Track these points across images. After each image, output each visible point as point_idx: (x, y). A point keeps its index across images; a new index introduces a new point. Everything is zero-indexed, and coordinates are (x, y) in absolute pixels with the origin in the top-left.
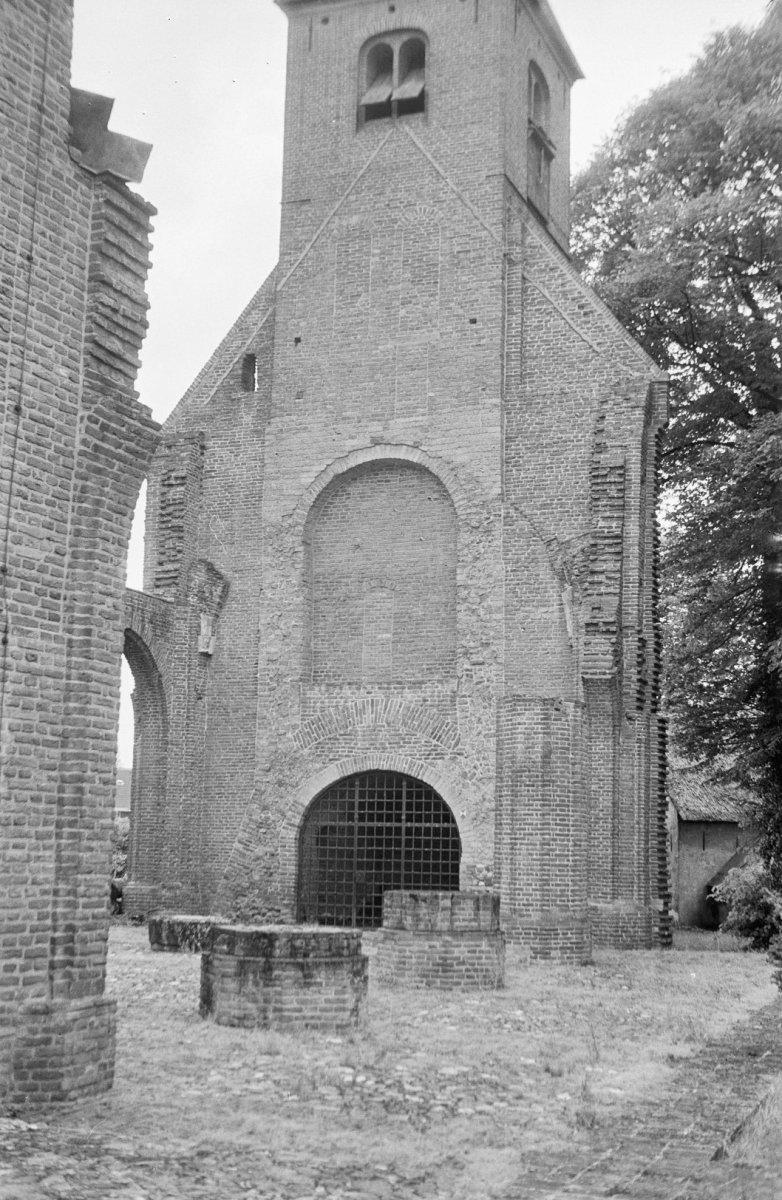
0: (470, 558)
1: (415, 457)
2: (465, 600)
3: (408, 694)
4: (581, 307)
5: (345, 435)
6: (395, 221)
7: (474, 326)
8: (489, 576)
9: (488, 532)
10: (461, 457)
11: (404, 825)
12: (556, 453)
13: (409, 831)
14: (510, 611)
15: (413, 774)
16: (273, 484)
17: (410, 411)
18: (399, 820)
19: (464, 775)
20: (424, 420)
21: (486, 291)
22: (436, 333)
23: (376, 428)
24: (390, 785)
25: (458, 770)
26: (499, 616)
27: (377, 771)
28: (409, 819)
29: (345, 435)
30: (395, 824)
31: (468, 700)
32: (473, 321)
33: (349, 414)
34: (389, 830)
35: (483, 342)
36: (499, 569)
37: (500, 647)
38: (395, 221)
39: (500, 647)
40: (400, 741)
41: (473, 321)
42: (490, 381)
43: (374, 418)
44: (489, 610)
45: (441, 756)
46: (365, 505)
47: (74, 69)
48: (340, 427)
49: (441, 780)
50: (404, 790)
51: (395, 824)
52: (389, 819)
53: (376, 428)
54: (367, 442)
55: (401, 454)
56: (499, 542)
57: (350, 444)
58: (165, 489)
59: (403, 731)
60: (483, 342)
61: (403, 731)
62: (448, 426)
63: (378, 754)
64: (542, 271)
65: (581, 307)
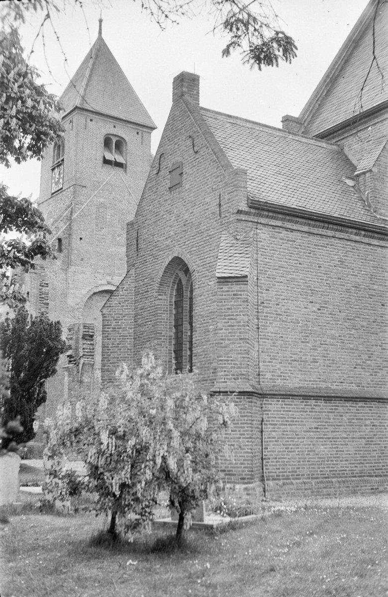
16: (72, 291)
23: (109, 278)
43: (109, 275)
48: (97, 275)
53: (109, 278)
54: (106, 283)
57: (100, 282)
58: (41, 288)
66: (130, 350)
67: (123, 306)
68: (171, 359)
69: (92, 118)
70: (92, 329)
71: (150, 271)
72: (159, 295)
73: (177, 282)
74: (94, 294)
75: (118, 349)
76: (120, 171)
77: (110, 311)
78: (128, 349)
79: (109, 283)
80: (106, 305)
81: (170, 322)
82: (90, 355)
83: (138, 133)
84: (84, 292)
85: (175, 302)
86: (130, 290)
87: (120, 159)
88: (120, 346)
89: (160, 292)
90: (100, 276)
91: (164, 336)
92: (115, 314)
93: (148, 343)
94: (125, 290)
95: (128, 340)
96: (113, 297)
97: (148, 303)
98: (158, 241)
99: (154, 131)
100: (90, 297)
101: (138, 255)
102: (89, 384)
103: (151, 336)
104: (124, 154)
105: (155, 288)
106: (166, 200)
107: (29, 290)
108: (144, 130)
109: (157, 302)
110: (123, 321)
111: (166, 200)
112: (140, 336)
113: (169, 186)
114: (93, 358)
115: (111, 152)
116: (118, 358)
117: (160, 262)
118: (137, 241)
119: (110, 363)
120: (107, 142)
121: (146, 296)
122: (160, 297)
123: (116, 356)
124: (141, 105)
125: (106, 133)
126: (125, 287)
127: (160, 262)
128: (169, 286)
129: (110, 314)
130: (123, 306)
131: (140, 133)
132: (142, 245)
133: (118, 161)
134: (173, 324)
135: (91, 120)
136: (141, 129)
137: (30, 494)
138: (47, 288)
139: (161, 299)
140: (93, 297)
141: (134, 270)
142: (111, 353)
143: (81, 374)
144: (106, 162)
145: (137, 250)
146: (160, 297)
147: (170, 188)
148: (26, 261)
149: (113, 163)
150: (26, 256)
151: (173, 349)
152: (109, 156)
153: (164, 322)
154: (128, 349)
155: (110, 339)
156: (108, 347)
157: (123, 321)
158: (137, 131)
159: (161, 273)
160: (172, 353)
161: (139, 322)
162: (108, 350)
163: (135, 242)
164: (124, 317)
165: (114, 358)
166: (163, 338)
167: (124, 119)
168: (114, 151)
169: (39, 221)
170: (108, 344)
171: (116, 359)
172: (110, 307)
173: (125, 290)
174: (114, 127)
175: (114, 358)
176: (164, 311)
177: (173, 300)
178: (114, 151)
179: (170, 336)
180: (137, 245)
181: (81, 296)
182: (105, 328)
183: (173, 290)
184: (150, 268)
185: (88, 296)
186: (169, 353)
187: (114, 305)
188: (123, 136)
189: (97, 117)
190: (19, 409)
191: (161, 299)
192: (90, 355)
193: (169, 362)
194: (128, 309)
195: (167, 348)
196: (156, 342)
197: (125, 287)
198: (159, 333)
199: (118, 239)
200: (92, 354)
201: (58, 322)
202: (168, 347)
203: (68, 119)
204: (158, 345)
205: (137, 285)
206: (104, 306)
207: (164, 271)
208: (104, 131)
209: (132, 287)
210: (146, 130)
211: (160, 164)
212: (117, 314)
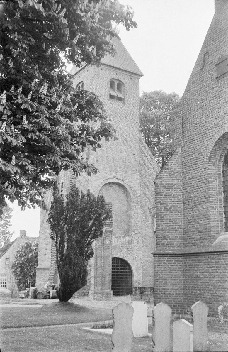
0: (134, 209)
1: (122, 183)
2: (133, 218)
3: (122, 239)
4: (150, 157)
5: (108, 174)
6: (118, 125)
7: (134, 156)
8: (138, 213)
9: (137, 203)
10: (132, 185)
11: (120, 271)
12: (148, 188)
13: (121, 272)
14: (142, 222)
15: (124, 258)
16: (91, 182)
17: (121, 172)
18: (119, 269)
19: (134, 259)
20: (124, 175)
21: (136, 148)
22: (127, 155)
23: (114, 174)
24: (117, 261)
25: (132, 258)
26: (140, 223)
27: (116, 257)
28: (121, 269)
29: (108, 174)
30: (118, 270)
31: (134, 242)
32: (134, 154)
33: (108, 169)
34: (117, 272)
35: (136, 160)
36: (140, 212)
37: (140, 230)
38: (118, 125)
39: (140, 230)
40: (121, 250)
41: (134, 154)
42: (137, 169)
43: (114, 172)
44: (138, 222)
45: (129, 254)
46: (107, 192)
47: (168, 91)
48: (106, 172)
49: (129, 259)
50: (120, 262)
51: (118, 270)
52: (117, 269)
53: (114, 174)
54: (112, 177)
55: (119, 182)
56: (139, 206)
57: (109, 177)
58: (71, 179)
59: (121, 248)
60: (136, 160)
61: (121, 248)
62: (129, 177)
63: (116, 253)
64: (143, 147)
65: (150, 157)
66: (180, 212)
67: (173, 177)
68: (222, 219)
69: (102, 68)
70: (110, 206)
71: (198, 147)
72: (209, 166)
73: (224, 155)
74: (105, 184)
75: (170, 212)
76: (120, 103)
77: (161, 182)
78: (179, 212)
79: (114, 177)
80: (158, 177)
81: (219, 188)
82: (110, 225)
83: (131, 79)
84: (99, 183)
85: (222, 171)
86: (178, 164)
87: (120, 95)
88: (171, 209)
89: (209, 163)
90: (109, 173)
91: (215, 200)
92: (166, 184)
93: (200, 206)
94: (174, 164)
95: (178, 205)
96: (163, 170)
97: (197, 173)
98: (206, 122)
99: (142, 78)
100: (102, 187)
101: (183, 136)
102: (109, 245)
103: (203, 200)
104: (123, 92)
105: (205, 160)
106: (214, 88)
107: (63, 181)
108: (136, 76)
109: (207, 172)
110: (173, 189)
111: (214, 88)
112: (191, 201)
113: (215, 76)
114: (112, 227)
115: (114, 90)
116: (170, 219)
117: (209, 138)
118: (183, 125)
119: (164, 224)
120: (112, 84)
121: (195, 168)
122: (210, 167)
123: (169, 218)
124: (133, 60)
125: (111, 78)
126: (174, 162)
127: (209, 138)
128: (217, 158)
129: (162, 184)
130: (173, 177)
131: (133, 78)
132: (188, 127)
133: (119, 96)
134: (222, 189)
135: (102, 69)
136: (133, 76)
137: (100, 334)
138: (76, 180)
139: (211, 169)
140: (105, 187)
141: (180, 149)
142: (164, 215)
143: (104, 238)
144: (111, 97)
145: (183, 132)
146: (210, 167)
147: (216, 78)
148: (94, 142)
149: (116, 97)
150: (94, 138)
151: (223, 211)
152: (113, 93)
153: (214, 188)
154: (179, 212)
155: (163, 204)
156: (161, 210)
157: (173, 189)
158: (130, 77)
159: (211, 148)
160: (222, 214)
161: (189, 189)
162: (161, 213)
163: (181, 126)
164: (174, 186)
165: (167, 219)
166: (214, 201)
167: (123, 69)
168: (116, 91)
169: (100, 111)
170: (161, 208)
171: (168, 220)
172: (162, 178)
173: (174, 164)
174: (116, 74)
175: (167, 219)
176: (214, 179)
177: (221, 170)
178: (116, 91)
179: (220, 200)
180: (183, 128)
181: (97, 186)
182: (158, 195)
183: (221, 162)
184: (198, 144)
185: (101, 186)
186: (220, 214)
187: (164, 176)
188: (122, 80)
189: (105, 67)
190: (76, 262)
191: (211, 169)
192: (110, 225)
193: (220, 221)
194: (176, 179)
195: (218, 209)
196: (208, 204)
197: (174, 162)
198: (211, 197)
199: (120, 148)
200: (111, 224)
201: (103, 196)
202: (219, 209)
203: (86, 69)
204: (211, 207)
205: (184, 160)
206: (156, 178)
207: (214, 146)
208: (110, 77)
209: (179, 162)
210: (137, 77)
211: (204, 61)
212: (168, 184)
